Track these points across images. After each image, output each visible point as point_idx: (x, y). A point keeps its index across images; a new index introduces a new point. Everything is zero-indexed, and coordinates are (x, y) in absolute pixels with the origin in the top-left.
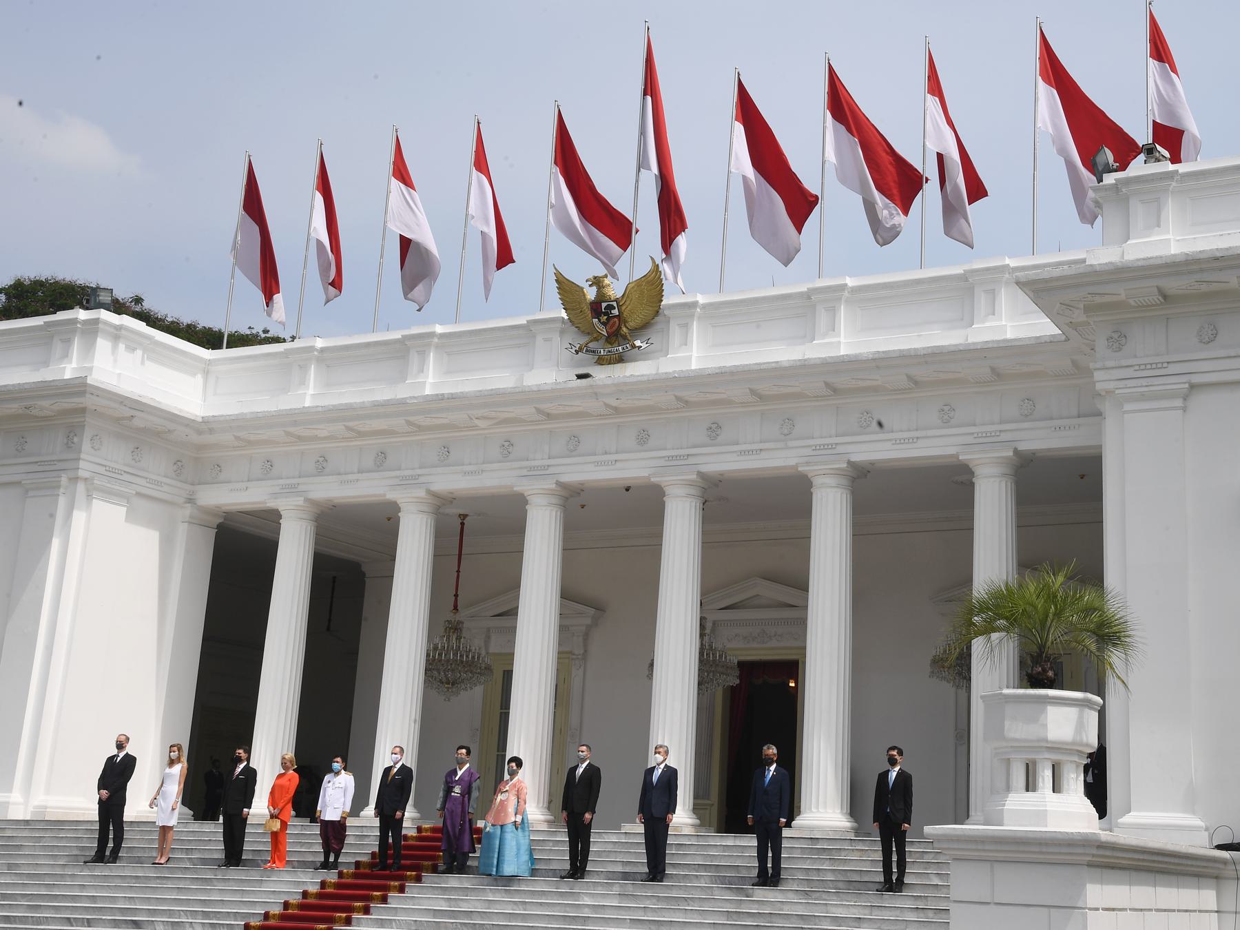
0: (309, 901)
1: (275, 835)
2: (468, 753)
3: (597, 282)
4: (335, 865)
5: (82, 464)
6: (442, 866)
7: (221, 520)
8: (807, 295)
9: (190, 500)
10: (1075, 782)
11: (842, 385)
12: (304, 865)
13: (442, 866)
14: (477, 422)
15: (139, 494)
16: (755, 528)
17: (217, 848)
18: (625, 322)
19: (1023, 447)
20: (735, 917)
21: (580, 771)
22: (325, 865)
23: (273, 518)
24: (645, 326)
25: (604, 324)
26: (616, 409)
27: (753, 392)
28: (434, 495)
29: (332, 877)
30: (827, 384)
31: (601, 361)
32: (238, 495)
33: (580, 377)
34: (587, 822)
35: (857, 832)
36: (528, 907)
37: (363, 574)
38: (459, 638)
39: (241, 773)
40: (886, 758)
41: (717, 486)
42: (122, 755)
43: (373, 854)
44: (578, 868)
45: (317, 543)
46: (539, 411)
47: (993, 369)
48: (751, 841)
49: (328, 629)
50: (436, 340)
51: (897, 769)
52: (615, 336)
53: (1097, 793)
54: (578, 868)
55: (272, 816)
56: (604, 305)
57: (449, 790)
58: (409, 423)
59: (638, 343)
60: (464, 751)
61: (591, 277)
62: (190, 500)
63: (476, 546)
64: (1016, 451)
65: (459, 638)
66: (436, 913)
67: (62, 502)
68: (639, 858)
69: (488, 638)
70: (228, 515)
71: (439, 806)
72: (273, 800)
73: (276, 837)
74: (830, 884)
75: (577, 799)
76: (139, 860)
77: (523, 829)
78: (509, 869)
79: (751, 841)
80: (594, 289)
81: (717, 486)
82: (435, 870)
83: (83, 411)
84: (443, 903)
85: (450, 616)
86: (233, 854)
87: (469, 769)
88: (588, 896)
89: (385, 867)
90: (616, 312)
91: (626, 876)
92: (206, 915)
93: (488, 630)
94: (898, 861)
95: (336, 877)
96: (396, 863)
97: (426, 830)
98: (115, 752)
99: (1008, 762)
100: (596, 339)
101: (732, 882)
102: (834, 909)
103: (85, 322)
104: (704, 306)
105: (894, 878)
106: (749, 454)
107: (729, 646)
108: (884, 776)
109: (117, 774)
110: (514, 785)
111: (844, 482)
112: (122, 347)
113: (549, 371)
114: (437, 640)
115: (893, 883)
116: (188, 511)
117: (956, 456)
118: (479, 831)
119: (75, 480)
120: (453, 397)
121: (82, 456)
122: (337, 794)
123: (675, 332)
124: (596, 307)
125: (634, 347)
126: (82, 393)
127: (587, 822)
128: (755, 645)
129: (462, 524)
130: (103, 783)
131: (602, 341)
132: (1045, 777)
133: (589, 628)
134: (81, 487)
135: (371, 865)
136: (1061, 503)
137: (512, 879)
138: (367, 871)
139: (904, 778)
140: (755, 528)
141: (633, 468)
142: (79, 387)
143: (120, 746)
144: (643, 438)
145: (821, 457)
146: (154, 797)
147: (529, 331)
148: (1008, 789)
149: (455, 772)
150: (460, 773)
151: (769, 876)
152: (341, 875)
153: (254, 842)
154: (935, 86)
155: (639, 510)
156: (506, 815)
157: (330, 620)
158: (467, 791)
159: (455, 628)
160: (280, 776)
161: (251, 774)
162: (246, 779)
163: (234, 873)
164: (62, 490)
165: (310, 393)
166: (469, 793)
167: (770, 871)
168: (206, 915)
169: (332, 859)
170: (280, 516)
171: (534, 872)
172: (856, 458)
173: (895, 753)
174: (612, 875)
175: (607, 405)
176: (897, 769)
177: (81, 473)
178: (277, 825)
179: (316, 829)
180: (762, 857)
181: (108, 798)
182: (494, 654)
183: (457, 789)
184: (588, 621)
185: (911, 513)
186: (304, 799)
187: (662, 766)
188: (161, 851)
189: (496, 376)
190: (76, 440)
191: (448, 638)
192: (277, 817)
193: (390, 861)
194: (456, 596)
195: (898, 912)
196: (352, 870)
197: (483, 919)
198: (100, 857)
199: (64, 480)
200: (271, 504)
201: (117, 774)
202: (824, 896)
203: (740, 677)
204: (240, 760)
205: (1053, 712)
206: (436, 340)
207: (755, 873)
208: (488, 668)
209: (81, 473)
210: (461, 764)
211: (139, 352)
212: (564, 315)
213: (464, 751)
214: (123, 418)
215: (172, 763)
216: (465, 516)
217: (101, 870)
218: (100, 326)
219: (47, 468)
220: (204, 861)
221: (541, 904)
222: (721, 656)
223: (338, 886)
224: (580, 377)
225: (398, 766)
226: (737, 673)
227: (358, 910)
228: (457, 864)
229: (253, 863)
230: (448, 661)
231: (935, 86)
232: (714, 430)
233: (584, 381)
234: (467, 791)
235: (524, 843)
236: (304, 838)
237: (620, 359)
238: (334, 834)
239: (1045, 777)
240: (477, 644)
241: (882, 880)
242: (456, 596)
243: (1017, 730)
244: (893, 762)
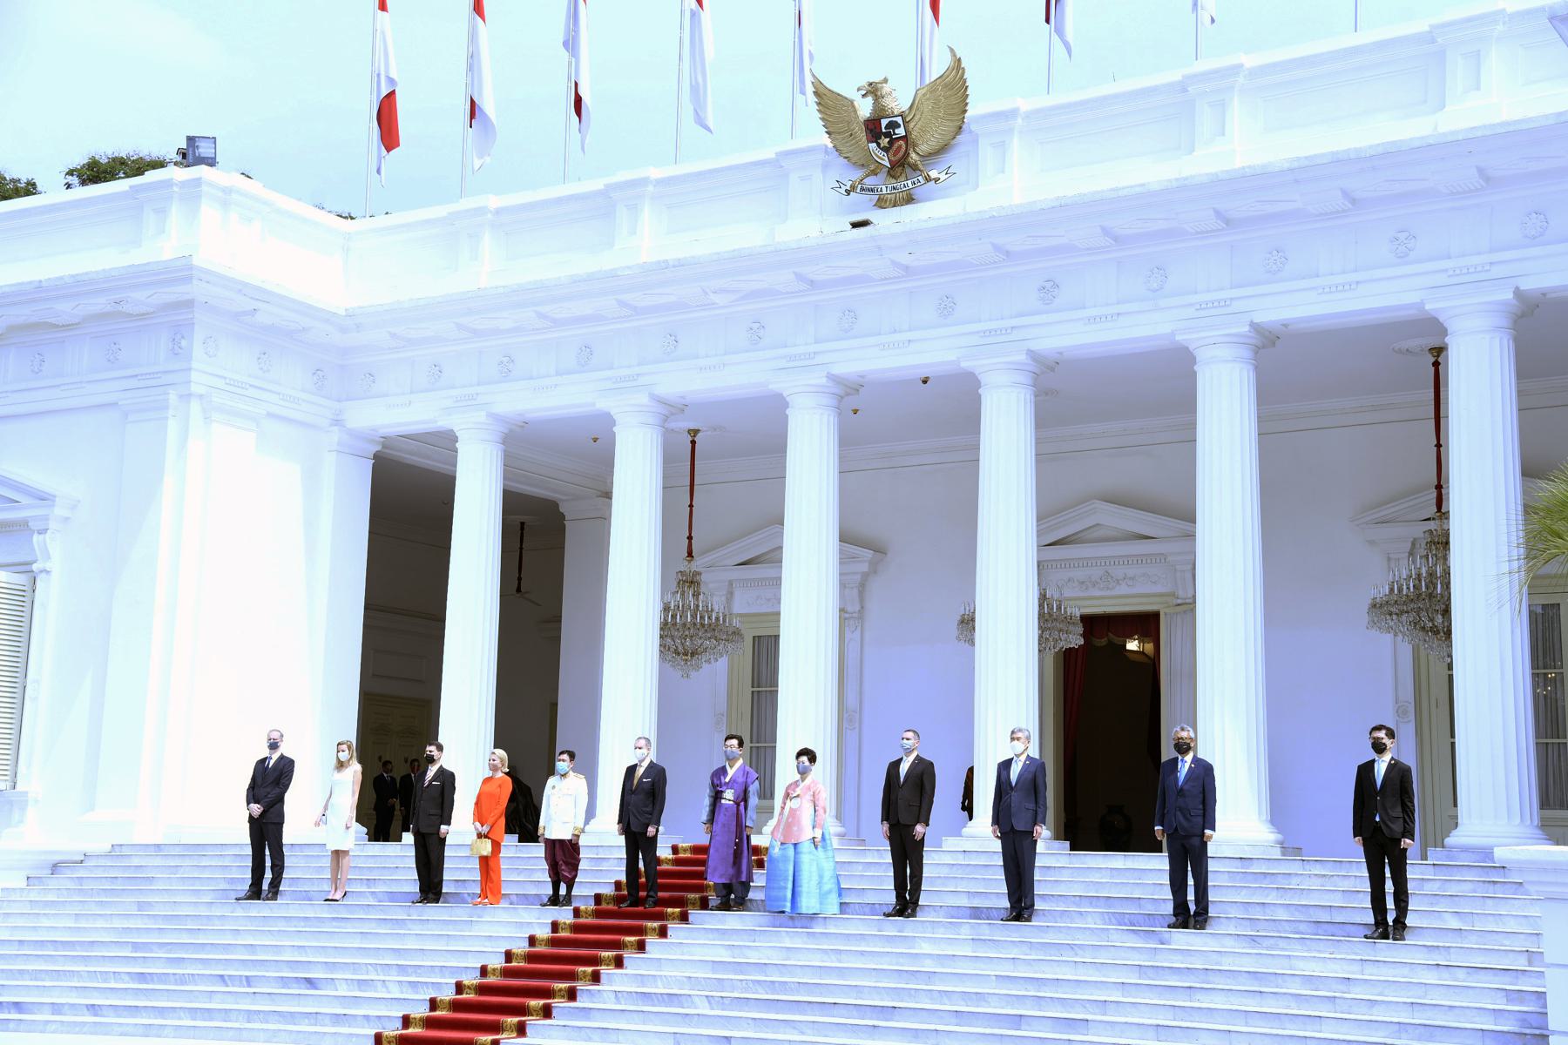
0: (538, 949)
1: (485, 861)
2: (741, 744)
3: (873, 90)
4: (568, 899)
5: (194, 376)
6: (714, 899)
7: (379, 448)
8: (1182, 87)
9: (337, 422)
11: (1243, 213)
12: (526, 899)
13: (714, 899)
14: (713, 297)
15: (270, 415)
16: (1114, 425)
17: (408, 878)
18: (915, 145)
19: (1528, 285)
20: (1150, 972)
21: (904, 768)
22: (555, 900)
23: (446, 442)
24: (943, 149)
25: (886, 150)
26: (906, 268)
27: (1106, 231)
29: (565, 915)
30: (1217, 213)
31: (881, 203)
32: (400, 413)
33: (855, 225)
34: (918, 838)
35: (1290, 849)
36: (844, 956)
37: (562, 517)
38: (696, 595)
39: (434, 779)
40: (1369, 743)
41: (1052, 369)
42: (275, 757)
43: (618, 885)
44: (906, 903)
45: (507, 476)
46: (799, 277)
47: (1481, 171)
48: (1157, 865)
49: (519, 590)
50: (650, 188)
51: (1387, 757)
52: (900, 166)
54: (906, 903)
55: (480, 836)
56: (884, 122)
57: (717, 796)
58: (622, 304)
59: (933, 174)
60: (735, 742)
61: (864, 83)
62: (337, 422)
63: (721, 469)
64: (1518, 293)
65: (696, 595)
66: (717, 965)
67: (173, 426)
68: (997, 891)
69: (730, 594)
70: (387, 441)
71: (704, 817)
72: (479, 816)
73: (488, 865)
74: (1287, 926)
75: (906, 803)
76: (307, 897)
77: (824, 847)
78: (808, 904)
79: (1157, 865)
80: (870, 100)
81: (1052, 369)
82: (704, 905)
83: (189, 304)
84: (723, 951)
85: (683, 566)
86: (431, 887)
87: (742, 768)
88: (924, 937)
89: (637, 902)
90: (901, 131)
91: (976, 913)
92: (402, 969)
93: (731, 583)
94: (1395, 893)
95: (571, 915)
96: (657, 893)
97: (685, 850)
98: (265, 753)
100: (874, 173)
101: (1138, 923)
102: (1301, 964)
103: (184, 184)
104: (1028, 116)
105: (1390, 919)
106: (1105, 320)
107: (1068, 593)
108: (1366, 770)
109: (270, 783)
110: (809, 788)
111: (1246, 353)
113: (815, 213)
114: (668, 597)
115: (1388, 924)
118: (757, 850)
119: (186, 397)
120: (680, 264)
121: (194, 365)
122: (563, 806)
123: (986, 152)
124: (873, 128)
125: (928, 179)
126: (188, 279)
127: (918, 838)
128: (1098, 593)
129: (693, 442)
130: (253, 794)
131: (883, 175)
133: (865, 577)
134: (195, 407)
135: (618, 900)
137: (813, 917)
138: (611, 907)
139: (1399, 773)
140: (1114, 425)
141: (931, 349)
142: (182, 272)
143: (274, 746)
144: (947, 308)
145: (1211, 322)
146: (325, 805)
147: (777, 169)
149: (723, 771)
150: (731, 772)
151: (1190, 913)
152: (577, 913)
153: (459, 867)
155: (950, 409)
156: (800, 830)
157: (520, 579)
158: (743, 798)
159: (690, 582)
160: (487, 781)
161: (447, 781)
162: (443, 786)
163: (432, 911)
164: (171, 412)
165: (489, 268)
166: (745, 800)
167: (1192, 908)
168: (402, 969)
169: (563, 891)
170: (456, 440)
171: (843, 906)
172: (1262, 318)
173: (1382, 734)
174: (956, 911)
175: (894, 263)
176: (1387, 757)
177: (194, 388)
178: (486, 848)
179: (538, 850)
180: (1178, 886)
181: (262, 815)
182: (741, 615)
183: (729, 795)
184: (864, 567)
186: (521, 815)
187: (1023, 758)
188: (335, 881)
189: (738, 231)
190: (184, 343)
191: (683, 594)
192: (486, 837)
193: (643, 894)
194: (690, 538)
195: (1406, 971)
196: (592, 907)
197: (782, 974)
198: (255, 892)
199: (173, 397)
200: (443, 423)
201: (270, 783)
202: (1281, 943)
203: (1084, 635)
204: (431, 760)
206: (650, 188)
207: (1169, 908)
208: (737, 633)
209: (194, 388)
210: (732, 760)
212: (826, 141)
213: (735, 742)
214: (245, 313)
215: (341, 765)
216: (696, 432)
217: (259, 908)
218: (205, 188)
219: (154, 382)
220: (393, 896)
221: (862, 953)
222: (1059, 608)
223: (576, 928)
224: (855, 225)
225: (645, 764)
226: (1080, 630)
227: (607, 962)
228: (733, 897)
229: (457, 898)
230: (684, 625)
232: (1049, 289)
233: (862, 230)
234: (743, 798)
235: (828, 867)
236: (525, 865)
237: (909, 199)
238: (563, 858)
240: (718, 605)
241: (1371, 920)
242: (690, 538)
244: (1379, 748)
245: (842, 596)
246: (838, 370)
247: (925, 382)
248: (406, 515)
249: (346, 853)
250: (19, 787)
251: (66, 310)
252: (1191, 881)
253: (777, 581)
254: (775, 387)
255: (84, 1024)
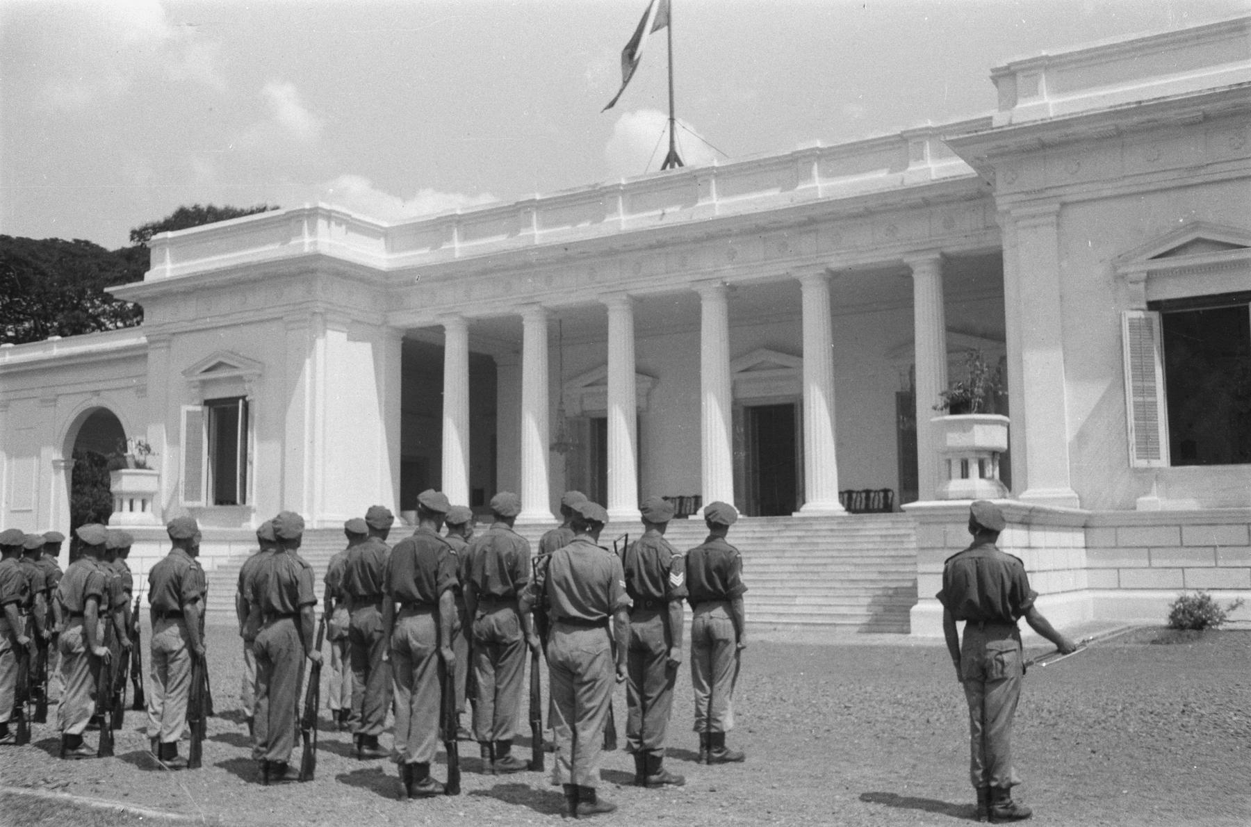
10: (993, 470)
11: (812, 221)
23: (440, 330)
28: (546, 309)
32: (417, 317)
53: (1006, 479)
62: (385, 323)
63: (576, 340)
70: (409, 331)
99: (949, 462)
111: (626, 307)
112: (333, 223)
117: (901, 260)
132: (974, 469)
136: (976, 293)
145: (710, 278)
148: (950, 478)
154: (612, 105)
185: (873, 305)
205: (977, 428)
211: (344, 227)
231: (612, 105)
239: (974, 469)
243: (955, 440)
245: (638, 400)
246: (634, 293)
248: (418, 367)
249: (384, 538)
250: (248, 503)
251: (175, 288)
252: (578, 596)
253: (606, 393)
254: (602, 301)
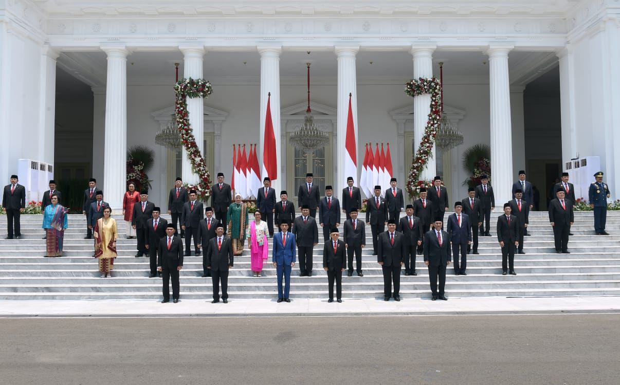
23: (100, 60)
32: (80, 40)
37: (93, 92)
116: (46, 48)
117: (99, 47)
159: (293, 253)
216: (442, 63)
247: (309, 53)
255: (463, 293)
